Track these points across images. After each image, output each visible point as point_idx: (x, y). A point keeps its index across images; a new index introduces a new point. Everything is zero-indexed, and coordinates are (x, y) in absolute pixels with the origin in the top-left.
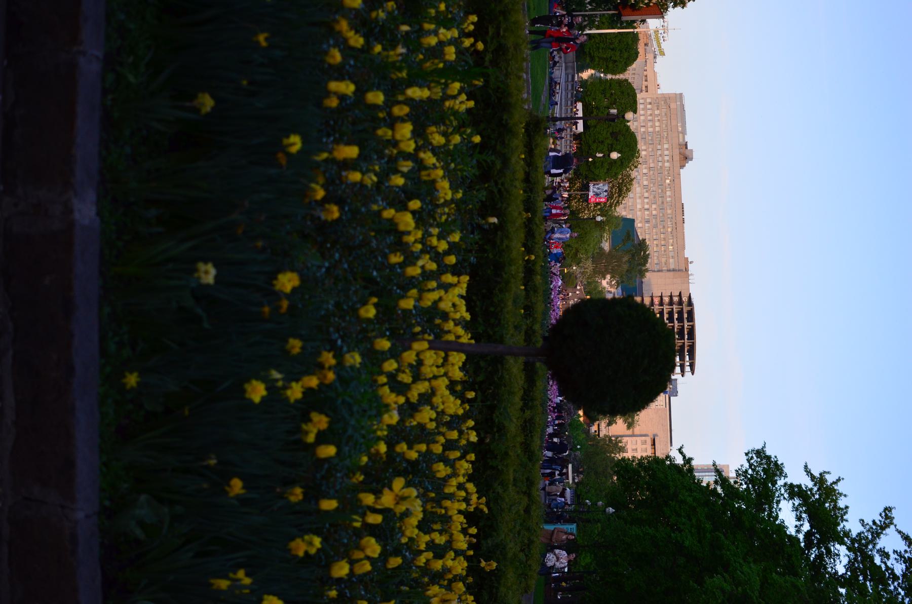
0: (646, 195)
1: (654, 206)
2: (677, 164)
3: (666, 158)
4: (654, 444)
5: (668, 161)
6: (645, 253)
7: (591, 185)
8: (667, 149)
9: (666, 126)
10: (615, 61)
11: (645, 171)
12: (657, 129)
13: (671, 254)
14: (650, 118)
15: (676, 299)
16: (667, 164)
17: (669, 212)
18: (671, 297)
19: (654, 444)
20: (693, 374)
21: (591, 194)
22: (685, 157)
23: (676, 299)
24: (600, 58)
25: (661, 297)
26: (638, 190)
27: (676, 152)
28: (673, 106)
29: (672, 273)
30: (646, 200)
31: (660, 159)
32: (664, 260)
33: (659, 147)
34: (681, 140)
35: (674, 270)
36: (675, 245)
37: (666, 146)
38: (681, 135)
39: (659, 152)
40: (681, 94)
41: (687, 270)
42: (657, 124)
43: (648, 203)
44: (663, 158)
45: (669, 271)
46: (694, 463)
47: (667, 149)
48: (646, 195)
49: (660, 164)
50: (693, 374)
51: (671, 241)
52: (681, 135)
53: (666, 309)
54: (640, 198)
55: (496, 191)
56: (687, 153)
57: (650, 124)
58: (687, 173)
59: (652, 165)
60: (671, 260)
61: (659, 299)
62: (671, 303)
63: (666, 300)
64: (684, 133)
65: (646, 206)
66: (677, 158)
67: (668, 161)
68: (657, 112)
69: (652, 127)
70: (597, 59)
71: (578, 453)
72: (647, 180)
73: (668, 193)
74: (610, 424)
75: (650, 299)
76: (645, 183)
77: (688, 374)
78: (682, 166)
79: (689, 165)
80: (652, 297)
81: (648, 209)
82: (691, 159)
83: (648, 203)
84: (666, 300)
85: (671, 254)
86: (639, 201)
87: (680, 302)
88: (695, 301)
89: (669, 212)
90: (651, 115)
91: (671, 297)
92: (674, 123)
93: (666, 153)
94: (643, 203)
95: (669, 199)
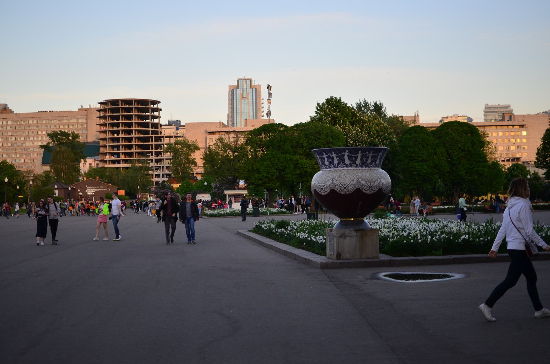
0: (31, 138)
1: (40, 133)
2: (9, 115)
3: (4, 123)
4: (212, 133)
5: (7, 122)
6: (59, 134)
11: (14, 139)
13: (75, 121)
15: (102, 114)
16: (9, 123)
17: (44, 122)
18: (100, 118)
19: (212, 133)
20: (159, 102)
23: (102, 114)
25: (101, 125)
26: (27, 144)
29: (88, 120)
30: (35, 138)
31: (5, 128)
32: (80, 127)
35: (86, 119)
36: (69, 118)
41: (86, 110)
43: (37, 137)
44: (5, 126)
45: (87, 123)
46: (241, 219)
48: (31, 138)
49: (9, 128)
50: (159, 102)
51: (66, 121)
53: (109, 121)
54: (33, 143)
55: (271, 218)
59: (9, 134)
60: (80, 121)
61: (102, 127)
62: (104, 117)
63: (102, 121)
65: (40, 138)
66: (4, 115)
67: (7, 122)
71: (213, 185)
72: (20, 138)
73: (31, 122)
74: (195, 164)
75: (102, 134)
76: (22, 139)
77: (160, 106)
78: (11, 112)
79: (10, 107)
80: (100, 132)
81: (42, 137)
82: (6, 105)
83: (37, 137)
84: (102, 121)
85: (75, 121)
86: (36, 144)
87: (104, 110)
88: (102, 100)
89: (44, 122)
91: (100, 118)
94: (37, 141)
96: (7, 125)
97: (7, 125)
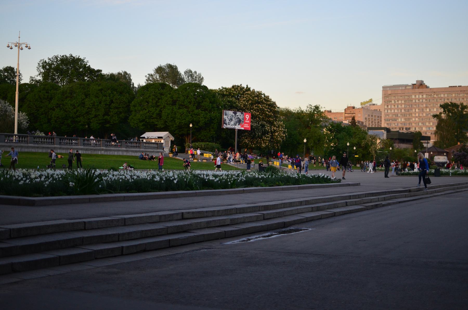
3: (421, 97)
7: (225, 126)
8: (415, 96)
9: (401, 96)
10: (112, 102)
11: (428, 110)
12: (403, 102)
14: (396, 107)
16: (424, 96)
17: (454, 95)
21: (238, 127)
22: (421, 85)
24: (106, 114)
27: (417, 90)
28: (389, 92)
31: (421, 100)
33: (414, 101)
34: (410, 87)
37: (413, 97)
38: (407, 88)
39: (417, 101)
40: (383, 87)
42: (400, 102)
47: (415, 96)
49: (424, 101)
52: (407, 88)
56: (418, 84)
57: (400, 106)
58: (431, 84)
59: (425, 106)
64: (406, 86)
66: (421, 90)
68: (393, 102)
69: (401, 105)
70: (106, 117)
72: (433, 109)
73: (442, 96)
78: (427, 87)
79: (426, 83)
82: (422, 81)
89: (454, 95)
90: (394, 106)
92: (400, 92)
93: (417, 97)
95: (446, 96)
96: (423, 98)
97: (423, 98)
